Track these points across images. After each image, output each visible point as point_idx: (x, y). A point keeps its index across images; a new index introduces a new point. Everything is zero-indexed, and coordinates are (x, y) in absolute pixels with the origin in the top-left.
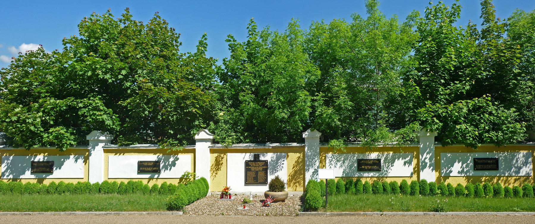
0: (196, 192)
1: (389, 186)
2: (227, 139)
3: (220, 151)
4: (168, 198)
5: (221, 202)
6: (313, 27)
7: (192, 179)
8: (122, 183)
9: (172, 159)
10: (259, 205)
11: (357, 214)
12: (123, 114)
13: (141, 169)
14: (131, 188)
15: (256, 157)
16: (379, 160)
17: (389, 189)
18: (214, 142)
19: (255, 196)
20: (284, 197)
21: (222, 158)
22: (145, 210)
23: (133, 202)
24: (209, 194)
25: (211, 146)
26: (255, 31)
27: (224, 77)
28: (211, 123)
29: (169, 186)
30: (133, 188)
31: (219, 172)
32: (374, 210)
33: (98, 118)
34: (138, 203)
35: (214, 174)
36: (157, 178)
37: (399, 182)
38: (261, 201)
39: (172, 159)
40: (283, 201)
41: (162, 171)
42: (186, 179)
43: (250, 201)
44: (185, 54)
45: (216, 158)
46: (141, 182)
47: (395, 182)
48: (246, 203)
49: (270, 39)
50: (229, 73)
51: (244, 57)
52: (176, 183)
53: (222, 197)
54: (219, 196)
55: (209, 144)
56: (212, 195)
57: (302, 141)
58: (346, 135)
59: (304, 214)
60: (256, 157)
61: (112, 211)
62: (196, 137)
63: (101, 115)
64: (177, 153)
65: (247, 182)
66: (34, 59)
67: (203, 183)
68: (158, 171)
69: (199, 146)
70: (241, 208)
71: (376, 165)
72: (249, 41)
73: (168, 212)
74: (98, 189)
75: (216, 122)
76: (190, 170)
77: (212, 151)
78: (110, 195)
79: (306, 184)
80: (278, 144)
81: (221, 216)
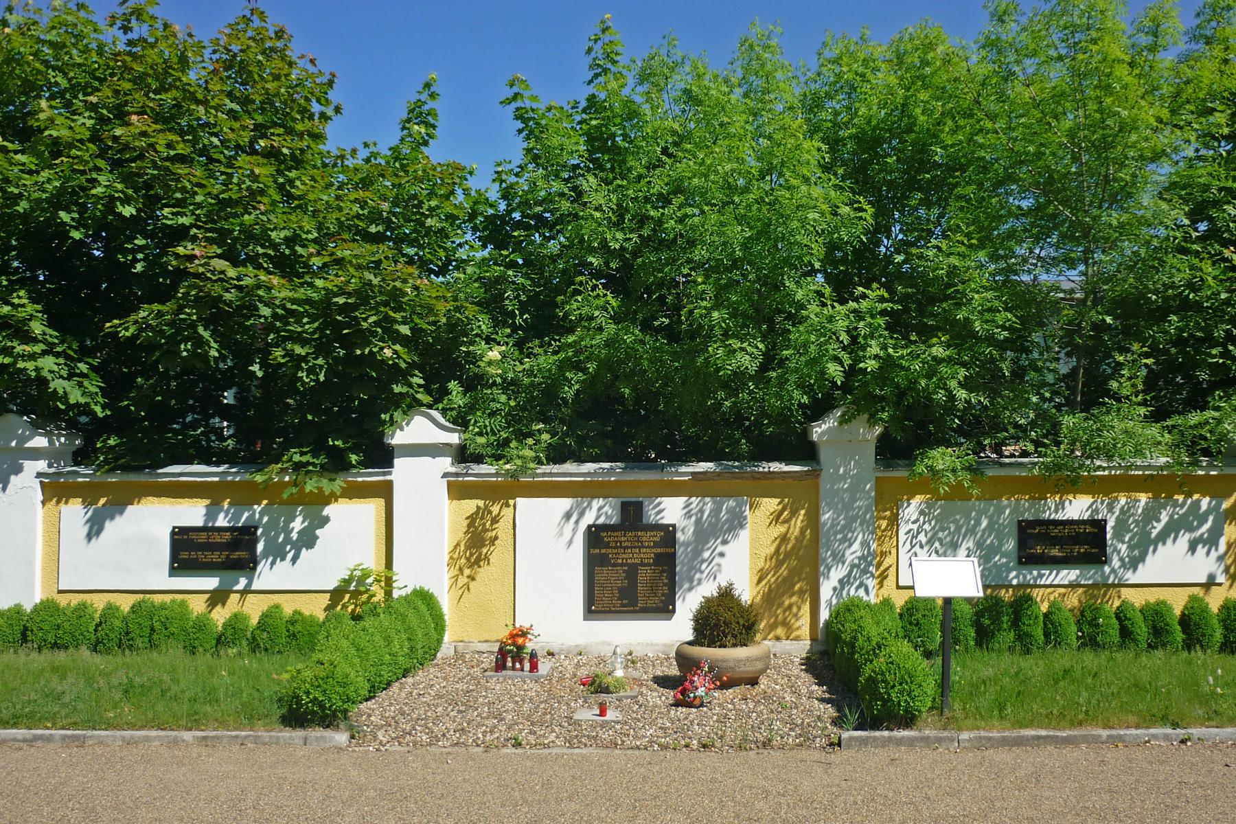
0: (399, 645)
1: (1139, 619)
2: (513, 444)
3: (485, 492)
4: (289, 673)
5: (498, 684)
6: (828, 54)
7: (380, 596)
8: (110, 609)
9: (298, 525)
10: (660, 698)
11: (1085, 739)
12: (119, 366)
13: (184, 555)
14: (135, 630)
15: (632, 514)
16: (1100, 525)
17: (1142, 630)
18: (463, 455)
19: (631, 660)
20: (760, 665)
21: (495, 520)
22: (194, 722)
23: (145, 690)
24: (446, 650)
25: (453, 470)
26: (614, 62)
27: (496, 232)
28: (453, 385)
29: (293, 622)
30: (152, 629)
31: (483, 572)
32: (1149, 720)
33: (21, 365)
34: (163, 693)
35: (463, 580)
36: (245, 592)
37: (1177, 602)
38: (663, 682)
39: (298, 525)
40: (754, 682)
41: (263, 566)
42: (356, 594)
43: (620, 685)
44: (354, 151)
45: (472, 519)
46: (183, 604)
47: (1164, 602)
48: (606, 690)
49: (679, 81)
50: (517, 215)
51: (576, 149)
52: (316, 608)
53: (500, 666)
54: (489, 661)
55: (445, 463)
56: (459, 656)
57: (807, 452)
58: (977, 429)
59: (864, 742)
60: (632, 514)
61: (54, 726)
62: (399, 438)
63: (33, 357)
64: (327, 500)
65: (595, 607)
66: (112, 442)
67: (423, 608)
68: (248, 565)
69: (403, 471)
70: (587, 715)
71: (1087, 543)
72: (592, 99)
73: (288, 734)
74: (18, 629)
75: (474, 383)
76: (372, 560)
77: (458, 491)
78: (61, 657)
79: (824, 615)
80: (710, 465)
81: (509, 750)
